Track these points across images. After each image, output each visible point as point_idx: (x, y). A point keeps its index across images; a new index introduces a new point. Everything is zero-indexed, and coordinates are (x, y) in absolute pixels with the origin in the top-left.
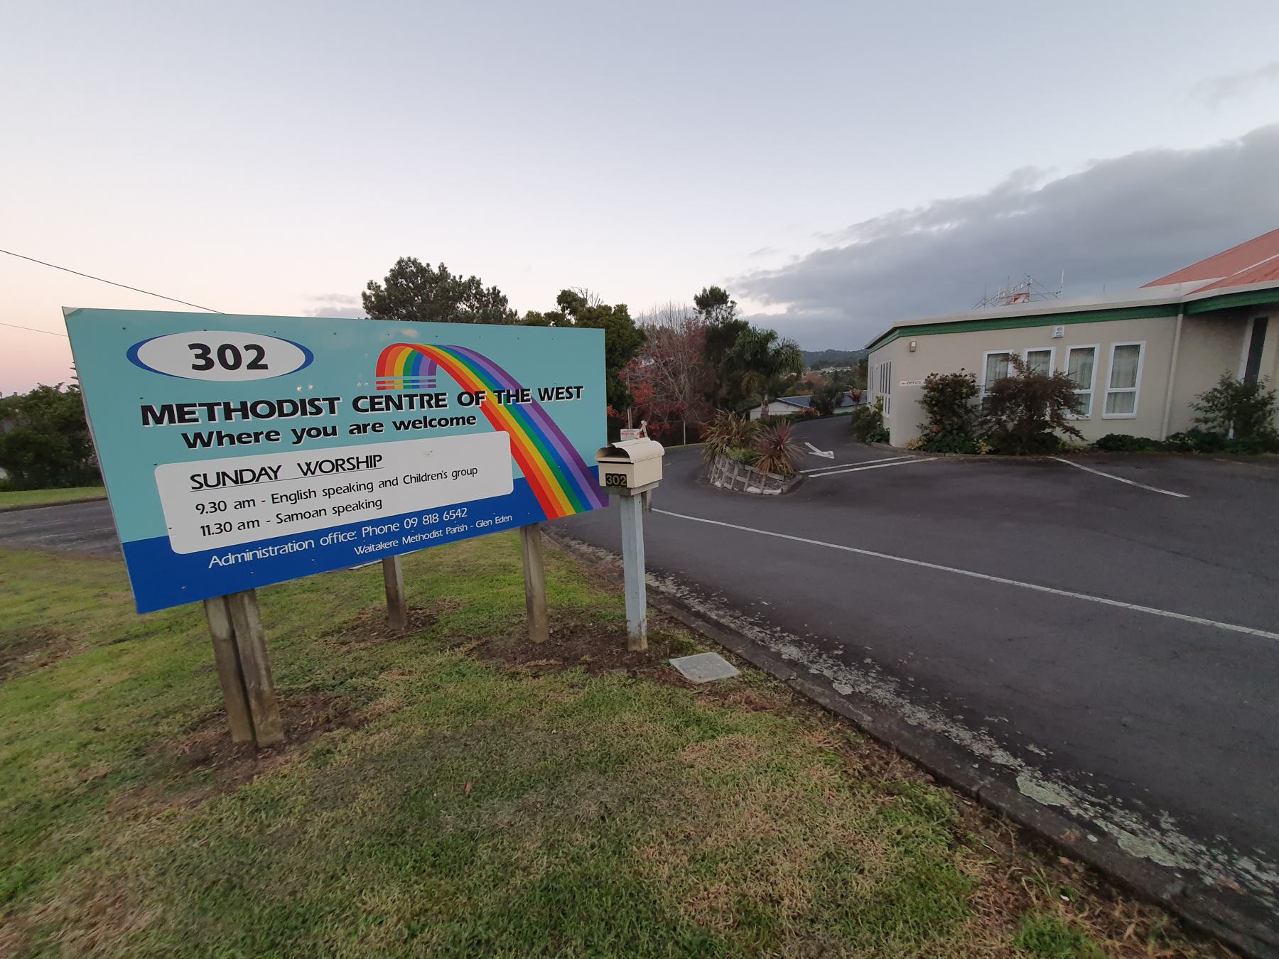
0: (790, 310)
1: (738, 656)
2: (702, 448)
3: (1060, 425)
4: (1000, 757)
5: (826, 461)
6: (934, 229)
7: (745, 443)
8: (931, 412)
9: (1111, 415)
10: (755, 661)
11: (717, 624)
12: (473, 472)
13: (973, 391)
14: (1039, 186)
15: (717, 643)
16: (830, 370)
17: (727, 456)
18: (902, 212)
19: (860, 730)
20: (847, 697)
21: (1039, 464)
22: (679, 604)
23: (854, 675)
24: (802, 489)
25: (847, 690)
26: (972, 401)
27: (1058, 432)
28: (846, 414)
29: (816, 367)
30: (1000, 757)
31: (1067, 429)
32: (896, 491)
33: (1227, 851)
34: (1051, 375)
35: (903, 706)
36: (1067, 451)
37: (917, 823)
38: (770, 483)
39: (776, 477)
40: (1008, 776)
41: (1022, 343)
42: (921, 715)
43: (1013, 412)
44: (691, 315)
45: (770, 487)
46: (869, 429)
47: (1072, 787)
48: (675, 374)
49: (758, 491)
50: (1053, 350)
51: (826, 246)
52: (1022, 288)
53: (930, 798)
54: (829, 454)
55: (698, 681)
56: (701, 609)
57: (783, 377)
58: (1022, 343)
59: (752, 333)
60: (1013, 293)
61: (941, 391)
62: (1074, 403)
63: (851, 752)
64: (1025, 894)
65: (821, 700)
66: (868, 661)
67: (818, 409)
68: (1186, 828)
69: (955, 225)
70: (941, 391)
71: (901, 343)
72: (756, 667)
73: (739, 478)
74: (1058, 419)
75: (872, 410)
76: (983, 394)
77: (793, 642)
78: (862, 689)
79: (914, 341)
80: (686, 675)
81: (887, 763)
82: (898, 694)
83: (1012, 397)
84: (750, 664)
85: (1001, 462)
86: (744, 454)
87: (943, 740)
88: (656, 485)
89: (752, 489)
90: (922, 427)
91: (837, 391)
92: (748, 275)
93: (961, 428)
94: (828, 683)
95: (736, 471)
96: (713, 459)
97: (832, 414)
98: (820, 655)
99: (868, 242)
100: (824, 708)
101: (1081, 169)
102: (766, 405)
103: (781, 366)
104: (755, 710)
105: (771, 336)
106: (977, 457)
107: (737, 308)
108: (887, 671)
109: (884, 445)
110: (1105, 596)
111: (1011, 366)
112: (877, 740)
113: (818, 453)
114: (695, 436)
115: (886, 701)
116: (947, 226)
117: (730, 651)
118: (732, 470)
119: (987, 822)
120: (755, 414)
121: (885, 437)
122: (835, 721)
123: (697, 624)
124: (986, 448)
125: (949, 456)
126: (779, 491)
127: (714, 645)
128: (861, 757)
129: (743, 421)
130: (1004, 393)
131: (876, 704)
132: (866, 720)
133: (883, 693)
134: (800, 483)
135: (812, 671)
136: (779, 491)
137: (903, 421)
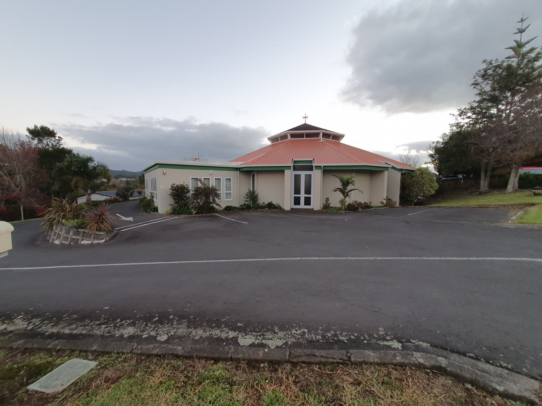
0: (98, 148)
1: (93, 352)
2: (41, 223)
3: (215, 203)
4: (232, 334)
5: (130, 222)
6: (165, 128)
7: (76, 217)
8: (174, 199)
9: (228, 200)
10: (108, 349)
11: (71, 337)
12: (450, 114)
13: (188, 191)
14: (197, 124)
15: (74, 351)
16: (125, 179)
17: (63, 225)
18: (151, 118)
19: (177, 357)
20: (166, 342)
21: (211, 216)
22: (32, 335)
23: (166, 328)
24: (117, 237)
25: (165, 337)
26: (189, 195)
27: (215, 206)
28: (135, 200)
29: (117, 177)
30: (232, 334)
31: (217, 204)
32: (163, 233)
33: (290, 330)
34: (211, 186)
35: (192, 332)
36: (217, 212)
37: (216, 390)
38: (97, 237)
39: (101, 233)
40: (235, 341)
41: (202, 175)
42: (200, 332)
43: (202, 199)
44: (26, 140)
45: (97, 239)
46: (148, 206)
47: (253, 333)
48: (11, 174)
49: (89, 242)
50: (210, 178)
51: (116, 123)
52: (197, 156)
53: (217, 373)
54: (131, 219)
55: (61, 389)
56: (55, 330)
57: (98, 181)
58: (202, 175)
59: (77, 157)
60: (194, 158)
61: (177, 191)
62: (218, 196)
63: (176, 373)
64: (257, 390)
65: (155, 352)
66: (171, 317)
67: (121, 197)
68: (282, 329)
69: (172, 129)
70: (177, 191)
71: (160, 170)
72: (108, 353)
73: (74, 237)
74: (214, 201)
75: (149, 198)
76: (191, 192)
77: (130, 325)
78: (172, 333)
79: (165, 170)
80: (47, 391)
81: (194, 367)
82: (188, 327)
83: (201, 193)
84: (104, 353)
85: (201, 217)
86: (77, 223)
87: (211, 339)
88: (6, 254)
89: (85, 242)
90: (171, 205)
91: (130, 189)
92: (68, 125)
93: (185, 205)
94: (154, 338)
95: (71, 233)
96: (51, 226)
97: (128, 200)
98: (147, 325)
99: (137, 126)
100: (157, 355)
101: (209, 123)
102: (89, 195)
103: (97, 176)
104: (112, 383)
105: (90, 159)
106: (192, 216)
107: (62, 142)
108: (181, 317)
109: (155, 213)
110: (240, 259)
111: (199, 182)
112: (186, 357)
113: (124, 218)
114: (31, 214)
115: (184, 334)
116: (169, 128)
117: (86, 351)
118: (68, 233)
119: (237, 368)
120: (81, 200)
121: (156, 210)
122: (164, 359)
123: (52, 344)
124: (194, 212)
125: (183, 216)
126: (104, 240)
127: (72, 353)
128: (182, 372)
129: (74, 204)
130: (198, 192)
131: (180, 338)
132: (179, 350)
133: (182, 330)
134: (116, 235)
135: (144, 337)
136: (104, 240)
137: (163, 203)
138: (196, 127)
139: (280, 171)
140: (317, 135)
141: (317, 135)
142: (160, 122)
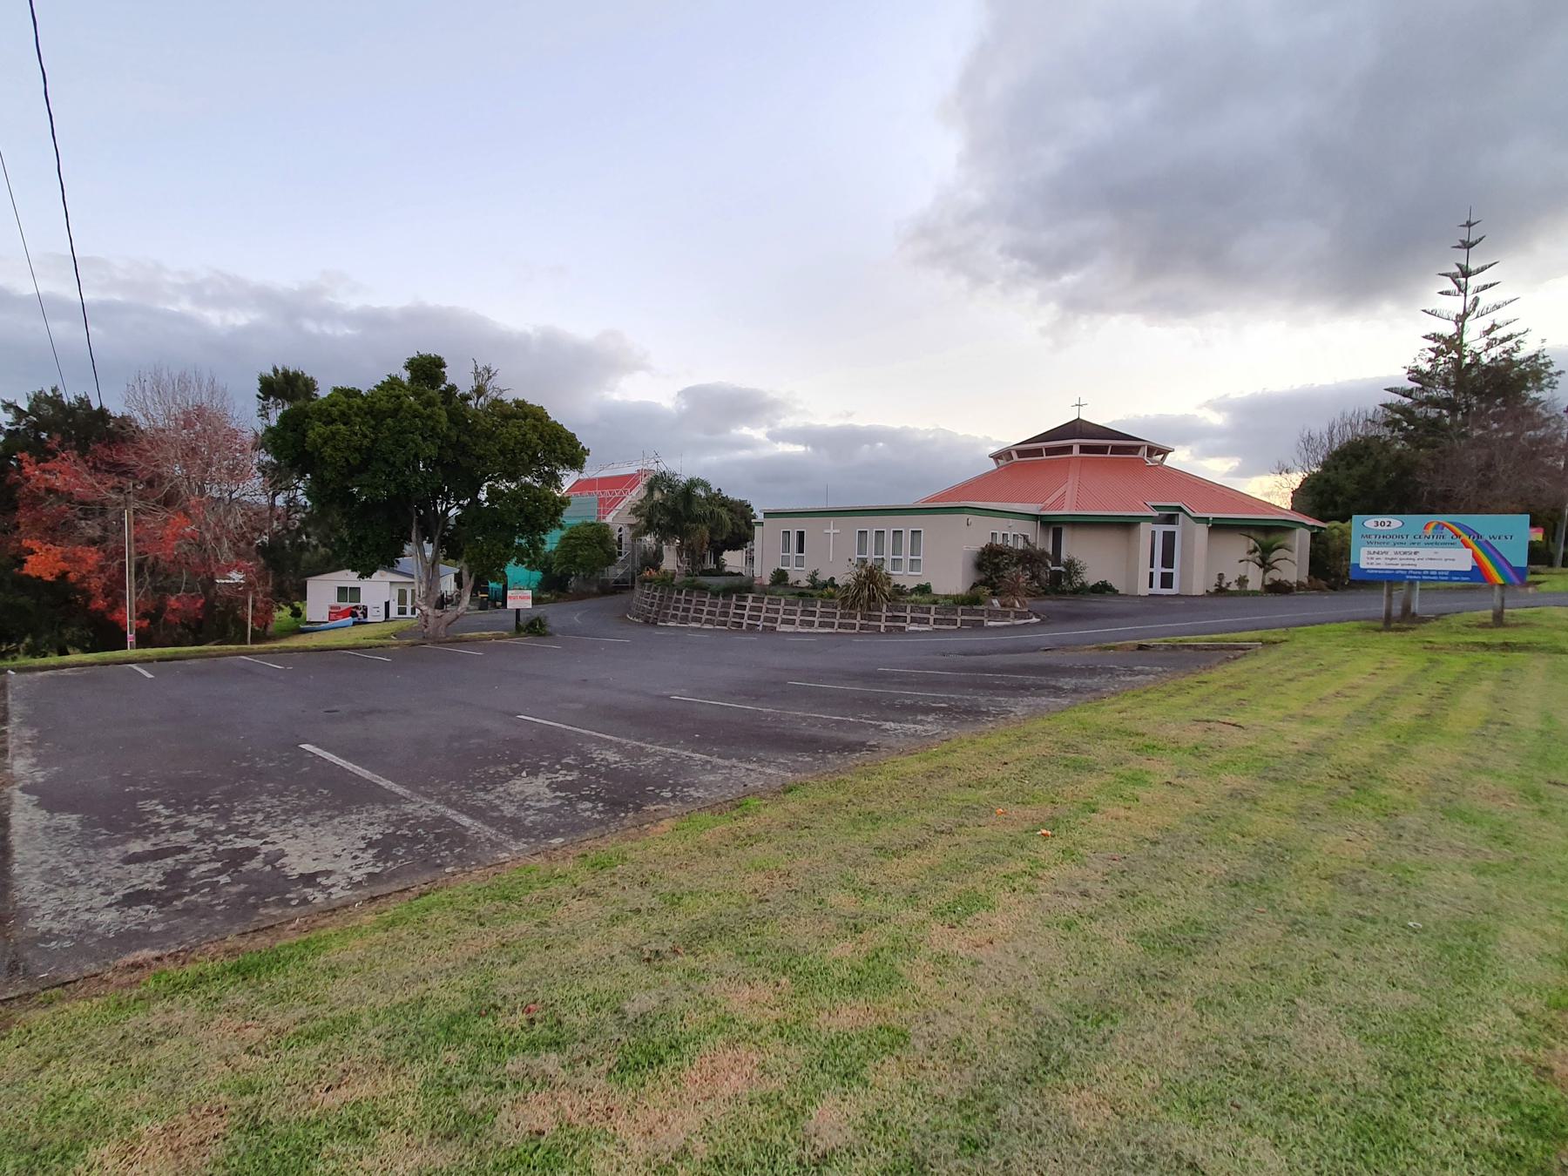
14: (354, 303)
79: (972, 518)
138: (350, 318)
139: (1126, 525)
140: (1139, 448)
141: (1139, 448)
142: (196, 291)
